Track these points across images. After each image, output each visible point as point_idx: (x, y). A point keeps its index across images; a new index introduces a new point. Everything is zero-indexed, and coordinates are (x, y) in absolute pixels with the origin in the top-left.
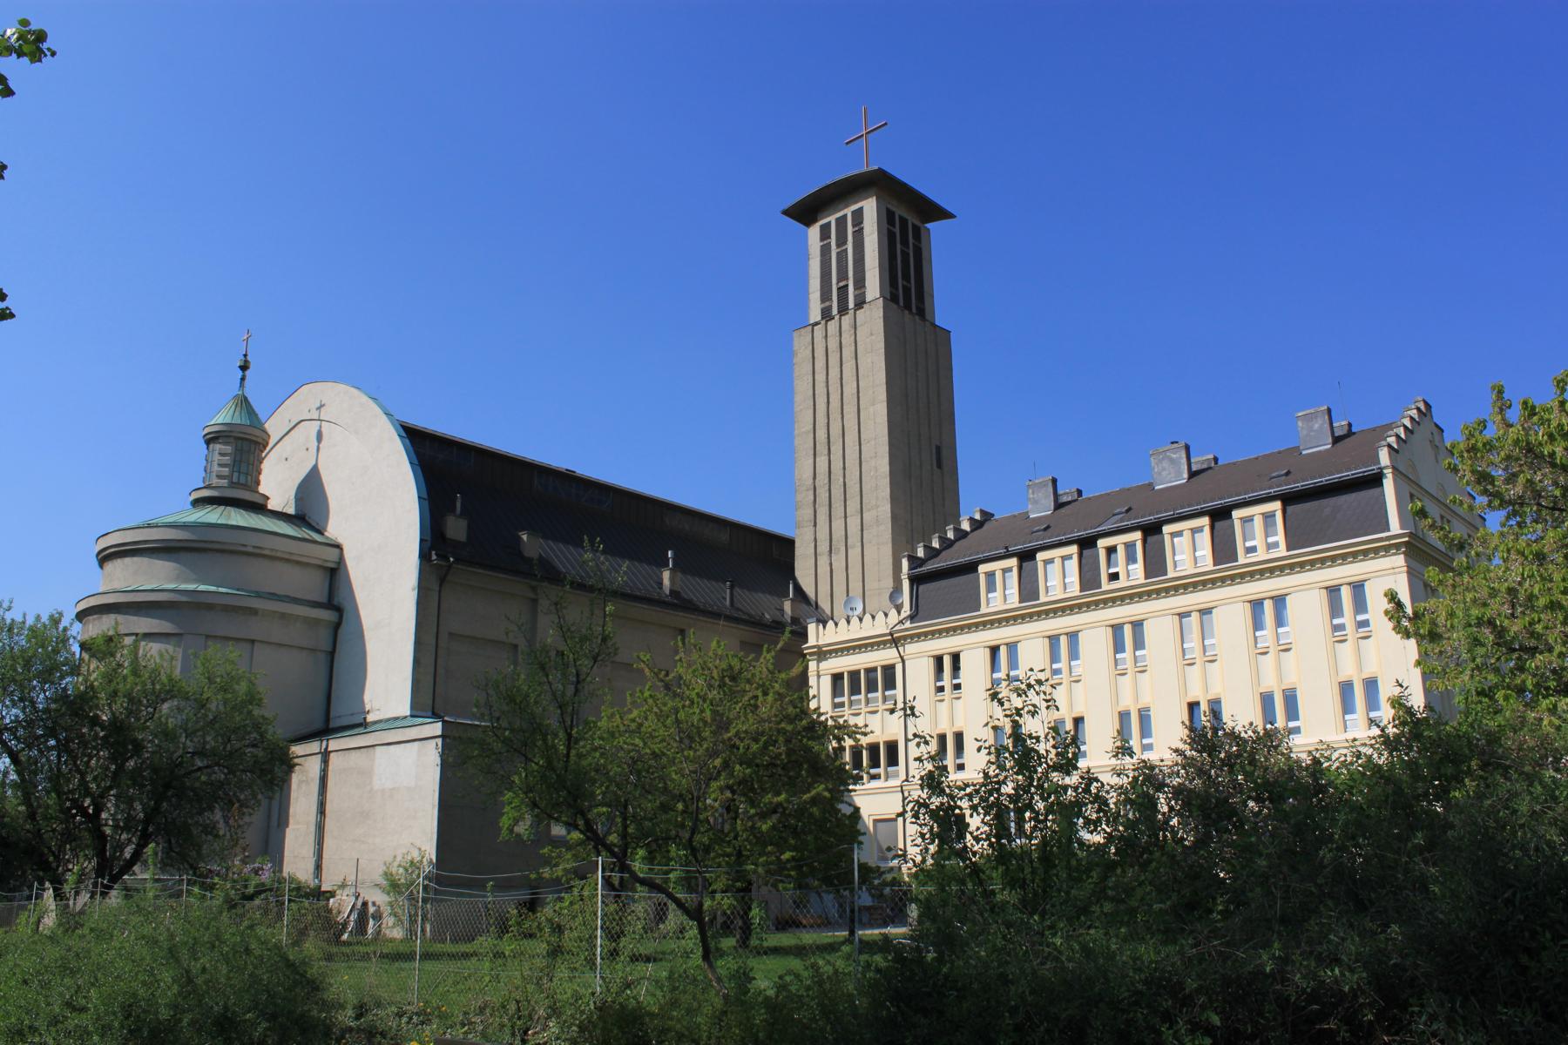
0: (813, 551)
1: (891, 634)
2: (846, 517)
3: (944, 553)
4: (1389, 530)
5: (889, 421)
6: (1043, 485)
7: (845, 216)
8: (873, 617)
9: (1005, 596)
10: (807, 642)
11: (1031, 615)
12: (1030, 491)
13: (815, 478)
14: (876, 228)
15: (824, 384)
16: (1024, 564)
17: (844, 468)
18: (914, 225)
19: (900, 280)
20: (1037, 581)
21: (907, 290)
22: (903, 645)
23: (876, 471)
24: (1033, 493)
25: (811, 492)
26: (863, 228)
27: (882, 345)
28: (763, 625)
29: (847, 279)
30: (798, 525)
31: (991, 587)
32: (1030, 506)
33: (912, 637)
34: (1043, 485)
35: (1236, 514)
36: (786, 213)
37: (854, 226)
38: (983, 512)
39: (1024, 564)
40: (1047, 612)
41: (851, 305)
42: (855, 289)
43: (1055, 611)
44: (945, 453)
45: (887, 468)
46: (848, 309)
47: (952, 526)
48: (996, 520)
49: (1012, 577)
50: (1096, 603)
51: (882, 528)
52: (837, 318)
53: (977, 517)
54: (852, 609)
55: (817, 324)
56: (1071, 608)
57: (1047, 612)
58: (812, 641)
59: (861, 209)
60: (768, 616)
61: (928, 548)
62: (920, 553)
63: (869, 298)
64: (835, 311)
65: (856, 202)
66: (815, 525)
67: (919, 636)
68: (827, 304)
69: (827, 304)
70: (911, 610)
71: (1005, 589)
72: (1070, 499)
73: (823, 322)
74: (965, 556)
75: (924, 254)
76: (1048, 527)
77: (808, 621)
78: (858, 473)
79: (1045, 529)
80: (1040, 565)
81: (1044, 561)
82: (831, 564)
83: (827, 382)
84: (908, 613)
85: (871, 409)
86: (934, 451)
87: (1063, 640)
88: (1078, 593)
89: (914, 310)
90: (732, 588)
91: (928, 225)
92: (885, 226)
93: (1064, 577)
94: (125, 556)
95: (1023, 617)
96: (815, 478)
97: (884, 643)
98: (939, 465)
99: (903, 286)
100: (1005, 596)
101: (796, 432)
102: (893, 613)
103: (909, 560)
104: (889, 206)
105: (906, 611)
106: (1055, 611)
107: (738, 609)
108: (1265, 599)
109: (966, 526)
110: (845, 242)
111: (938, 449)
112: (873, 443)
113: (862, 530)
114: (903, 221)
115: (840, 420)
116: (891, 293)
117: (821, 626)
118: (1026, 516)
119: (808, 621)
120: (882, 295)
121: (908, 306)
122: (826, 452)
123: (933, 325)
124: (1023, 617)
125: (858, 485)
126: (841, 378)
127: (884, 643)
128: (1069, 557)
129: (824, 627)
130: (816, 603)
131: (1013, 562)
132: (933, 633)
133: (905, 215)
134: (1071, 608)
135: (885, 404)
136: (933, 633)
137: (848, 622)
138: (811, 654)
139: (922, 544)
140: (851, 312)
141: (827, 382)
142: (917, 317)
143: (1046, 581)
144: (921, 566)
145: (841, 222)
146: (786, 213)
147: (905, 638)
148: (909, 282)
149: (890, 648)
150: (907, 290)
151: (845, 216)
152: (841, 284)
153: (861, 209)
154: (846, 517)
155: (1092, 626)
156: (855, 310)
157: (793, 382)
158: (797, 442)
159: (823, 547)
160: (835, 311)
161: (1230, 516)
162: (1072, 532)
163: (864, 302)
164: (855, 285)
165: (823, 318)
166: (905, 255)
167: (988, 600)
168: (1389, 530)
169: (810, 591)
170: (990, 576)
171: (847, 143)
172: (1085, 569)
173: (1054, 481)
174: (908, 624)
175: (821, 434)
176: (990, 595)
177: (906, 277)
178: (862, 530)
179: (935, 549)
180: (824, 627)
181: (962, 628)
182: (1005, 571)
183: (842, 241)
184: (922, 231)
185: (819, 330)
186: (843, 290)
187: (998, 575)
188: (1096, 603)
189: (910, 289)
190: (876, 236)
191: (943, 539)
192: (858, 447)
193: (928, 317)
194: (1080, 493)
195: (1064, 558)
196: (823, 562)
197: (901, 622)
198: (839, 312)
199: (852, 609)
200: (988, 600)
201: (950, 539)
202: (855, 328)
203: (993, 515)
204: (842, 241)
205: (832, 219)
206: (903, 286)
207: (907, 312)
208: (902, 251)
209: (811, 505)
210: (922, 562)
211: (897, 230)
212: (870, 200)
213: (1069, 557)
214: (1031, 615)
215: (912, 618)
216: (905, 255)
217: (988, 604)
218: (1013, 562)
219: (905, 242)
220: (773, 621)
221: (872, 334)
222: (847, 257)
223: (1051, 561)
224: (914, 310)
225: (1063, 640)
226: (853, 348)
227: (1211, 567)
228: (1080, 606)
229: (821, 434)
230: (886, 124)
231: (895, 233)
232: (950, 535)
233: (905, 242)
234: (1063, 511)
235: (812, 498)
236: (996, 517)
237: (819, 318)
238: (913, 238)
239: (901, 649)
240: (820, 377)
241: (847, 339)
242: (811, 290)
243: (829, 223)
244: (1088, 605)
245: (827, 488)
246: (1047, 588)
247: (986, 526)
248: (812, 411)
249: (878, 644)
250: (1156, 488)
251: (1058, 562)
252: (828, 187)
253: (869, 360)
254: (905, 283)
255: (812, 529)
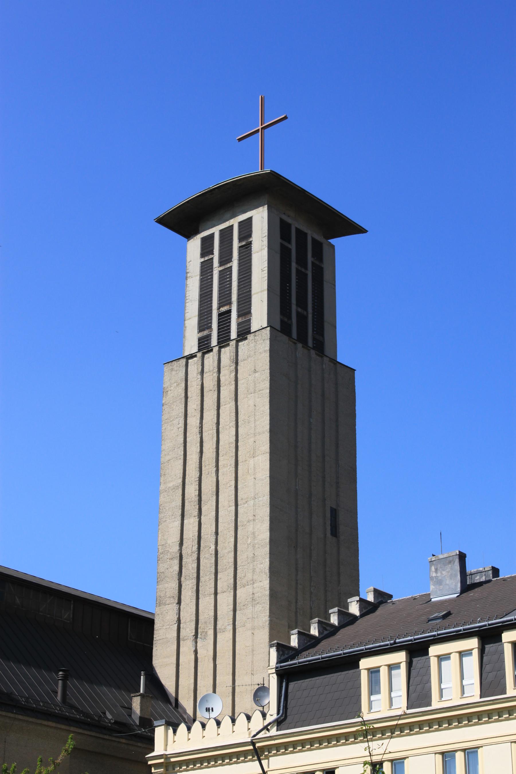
0: (175, 634)
1: (253, 743)
2: (216, 594)
3: (324, 643)
4: (505, 693)
5: (272, 477)
6: (448, 561)
7: (232, 227)
8: (204, 726)
9: (391, 699)
10: (153, 750)
11: (420, 725)
12: (433, 568)
13: (181, 544)
14: (266, 242)
15: (197, 430)
16: (415, 660)
17: (217, 533)
18: (314, 240)
19: (294, 307)
20: (429, 681)
21: (302, 319)
22: (267, 758)
23: (254, 538)
24: (436, 570)
25: (177, 562)
26: (250, 243)
27: (267, 384)
28: (105, 728)
29: (230, 303)
30: (159, 603)
31: (374, 688)
32: (432, 587)
33: (278, 747)
34: (448, 561)
35: (365, 663)
36: (162, 221)
37: (240, 240)
38: (377, 592)
39: (415, 660)
40: (440, 722)
41: (234, 335)
42: (239, 316)
43: (449, 720)
44: (342, 517)
45: (267, 535)
46: (229, 339)
47: (336, 609)
48: (393, 603)
49: (399, 675)
50: (500, 712)
51: (258, 608)
52: (216, 349)
53: (370, 598)
54: (208, 710)
55: (192, 356)
56: (469, 717)
57: (440, 722)
58: (159, 749)
59: (250, 219)
60: (109, 716)
61: (304, 636)
62: (294, 642)
63: (255, 326)
64: (214, 341)
65: (245, 212)
66: (179, 603)
67: (286, 746)
68: (206, 333)
69: (206, 333)
70: (278, 713)
71: (391, 690)
72: (483, 579)
73: (199, 355)
74: (345, 648)
75: (327, 276)
76: (448, 614)
77: (156, 723)
78: (233, 540)
79: (445, 617)
80: (434, 662)
81: (438, 657)
82: (196, 652)
83: (201, 427)
84: (275, 717)
85: (252, 462)
86: (328, 515)
87: (460, 757)
88: (477, 699)
89: (310, 343)
90: (65, 679)
91: (332, 241)
92: (279, 240)
93: (462, 678)
94: (201, 402)
95: (411, 726)
96: (181, 544)
97: (245, 754)
98: (335, 532)
99: (298, 313)
100: (391, 699)
101: (162, 487)
102: (257, 716)
103: (278, 651)
104: (285, 218)
105: (273, 714)
106: (449, 720)
107: (72, 707)
108: (456, 751)
109: (354, 609)
110: (229, 260)
111: (334, 513)
112: (251, 503)
113: (235, 610)
114: (301, 235)
115: (214, 474)
116: (282, 322)
117: (171, 731)
118: (426, 599)
119: (156, 723)
120: (270, 325)
121: (302, 338)
122: (196, 513)
123: (334, 361)
124: (411, 726)
125: (232, 555)
126: (218, 423)
127: (245, 754)
128: (468, 653)
129: (175, 732)
130: (177, 700)
131: (401, 657)
132: (303, 743)
133: (304, 228)
134: (469, 717)
135: (267, 456)
136: (303, 743)
137: (233, 721)
138: (157, 766)
139: (295, 631)
140: (233, 343)
141: (201, 427)
142: (313, 352)
143: (440, 681)
144: (292, 658)
145: (227, 234)
146: (162, 221)
147: (269, 748)
148: (305, 308)
149: (252, 760)
150: (302, 319)
151: (232, 227)
152: (223, 309)
153: (250, 219)
154: (216, 594)
155: (349, 762)
156: (238, 342)
157: (161, 426)
158: (162, 499)
159: (188, 630)
160: (214, 341)
161: (427, 653)
162: (474, 622)
163: (249, 332)
164: (238, 311)
165: (199, 350)
166: (302, 277)
167: (370, 703)
168: (505, 693)
169: (169, 684)
170: (374, 672)
171: (240, 140)
172: (487, 668)
173: (462, 557)
174: (274, 731)
175: (191, 490)
176: (373, 698)
177: (302, 302)
178: (235, 610)
179: (313, 637)
180: (175, 732)
181: (338, 738)
182: (391, 667)
183: (226, 257)
184: (325, 248)
185: (194, 365)
186: (224, 317)
187: (384, 672)
188: (500, 712)
189: (306, 318)
190: (265, 253)
191: (324, 625)
192: (233, 508)
193: (328, 351)
194: (496, 572)
195: (462, 654)
196: (187, 648)
197: (266, 728)
198: (219, 343)
199: (208, 710)
200: (370, 703)
201: (332, 626)
202: (237, 363)
203: (391, 597)
204: (226, 257)
205: (216, 230)
206: (298, 314)
207: (300, 345)
208: (298, 271)
209: (176, 577)
210: (295, 653)
211: (293, 247)
212: (261, 209)
213: (468, 653)
214: (420, 725)
215: (279, 723)
216: (302, 277)
217: (441, 696)
218: (401, 657)
219: (302, 261)
220: (116, 723)
221: (255, 371)
222: (231, 277)
223: (445, 657)
224: (310, 343)
225: (460, 757)
226: (233, 387)
227: (477, 699)
228: (479, 716)
229: (191, 490)
230: (285, 118)
231: (290, 250)
232: (334, 620)
233: (302, 261)
234: (471, 594)
235: (177, 568)
236: (394, 599)
237: (195, 349)
238: (313, 256)
239: (264, 762)
240: (193, 421)
241: (227, 376)
242: (187, 316)
243: (212, 236)
244: (489, 714)
245: (195, 556)
246: (441, 691)
247: (380, 611)
248: (181, 462)
249: (238, 755)
250: (433, 600)
251: (455, 657)
252: (211, 192)
253: (251, 403)
254: (300, 310)
255: (175, 607)
